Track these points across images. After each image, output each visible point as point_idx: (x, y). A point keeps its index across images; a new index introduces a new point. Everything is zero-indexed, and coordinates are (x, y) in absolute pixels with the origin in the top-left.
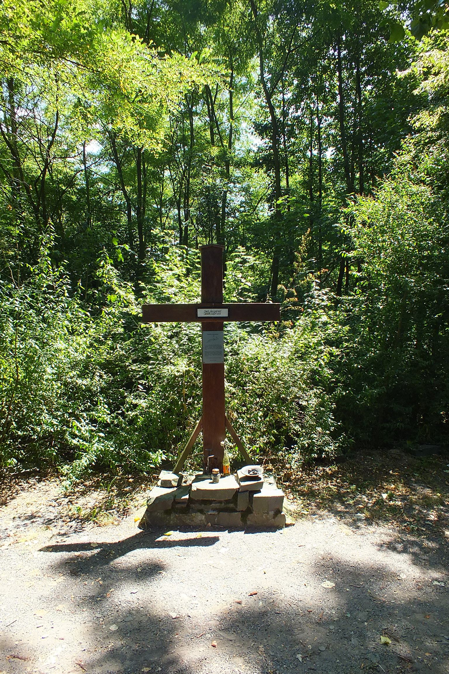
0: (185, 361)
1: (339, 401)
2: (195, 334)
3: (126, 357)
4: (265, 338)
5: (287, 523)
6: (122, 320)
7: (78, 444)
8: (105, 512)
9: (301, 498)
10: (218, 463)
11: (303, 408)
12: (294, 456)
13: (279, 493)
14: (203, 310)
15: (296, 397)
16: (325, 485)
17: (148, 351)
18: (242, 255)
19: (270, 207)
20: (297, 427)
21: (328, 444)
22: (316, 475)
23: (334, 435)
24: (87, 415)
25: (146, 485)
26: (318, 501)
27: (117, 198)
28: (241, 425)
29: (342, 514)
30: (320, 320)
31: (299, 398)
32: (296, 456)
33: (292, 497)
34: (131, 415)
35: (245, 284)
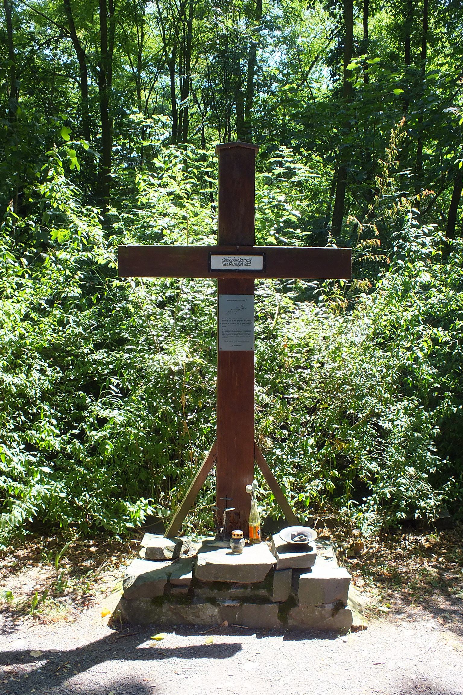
0: (187, 348)
1: (447, 422)
2: (203, 301)
3: (83, 339)
4: (323, 309)
5: (354, 624)
6: (79, 273)
7: (5, 485)
8: (52, 600)
9: (378, 584)
10: (241, 521)
11: (384, 433)
12: (367, 515)
13: (342, 573)
14: (221, 257)
15: (373, 414)
16: (418, 566)
17: (121, 329)
18: (286, 161)
19: (333, 74)
20: (374, 464)
21: (425, 496)
22: (404, 549)
23: (436, 481)
24: (19, 437)
25: (119, 557)
26: (406, 590)
27: (62, 53)
28: (279, 460)
29: (447, 615)
30: (418, 279)
31: (378, 416)
32: (372, 516)
33: (362, 583)
34: (96, 437)
35: (290, 214)
